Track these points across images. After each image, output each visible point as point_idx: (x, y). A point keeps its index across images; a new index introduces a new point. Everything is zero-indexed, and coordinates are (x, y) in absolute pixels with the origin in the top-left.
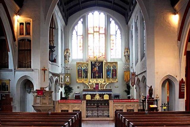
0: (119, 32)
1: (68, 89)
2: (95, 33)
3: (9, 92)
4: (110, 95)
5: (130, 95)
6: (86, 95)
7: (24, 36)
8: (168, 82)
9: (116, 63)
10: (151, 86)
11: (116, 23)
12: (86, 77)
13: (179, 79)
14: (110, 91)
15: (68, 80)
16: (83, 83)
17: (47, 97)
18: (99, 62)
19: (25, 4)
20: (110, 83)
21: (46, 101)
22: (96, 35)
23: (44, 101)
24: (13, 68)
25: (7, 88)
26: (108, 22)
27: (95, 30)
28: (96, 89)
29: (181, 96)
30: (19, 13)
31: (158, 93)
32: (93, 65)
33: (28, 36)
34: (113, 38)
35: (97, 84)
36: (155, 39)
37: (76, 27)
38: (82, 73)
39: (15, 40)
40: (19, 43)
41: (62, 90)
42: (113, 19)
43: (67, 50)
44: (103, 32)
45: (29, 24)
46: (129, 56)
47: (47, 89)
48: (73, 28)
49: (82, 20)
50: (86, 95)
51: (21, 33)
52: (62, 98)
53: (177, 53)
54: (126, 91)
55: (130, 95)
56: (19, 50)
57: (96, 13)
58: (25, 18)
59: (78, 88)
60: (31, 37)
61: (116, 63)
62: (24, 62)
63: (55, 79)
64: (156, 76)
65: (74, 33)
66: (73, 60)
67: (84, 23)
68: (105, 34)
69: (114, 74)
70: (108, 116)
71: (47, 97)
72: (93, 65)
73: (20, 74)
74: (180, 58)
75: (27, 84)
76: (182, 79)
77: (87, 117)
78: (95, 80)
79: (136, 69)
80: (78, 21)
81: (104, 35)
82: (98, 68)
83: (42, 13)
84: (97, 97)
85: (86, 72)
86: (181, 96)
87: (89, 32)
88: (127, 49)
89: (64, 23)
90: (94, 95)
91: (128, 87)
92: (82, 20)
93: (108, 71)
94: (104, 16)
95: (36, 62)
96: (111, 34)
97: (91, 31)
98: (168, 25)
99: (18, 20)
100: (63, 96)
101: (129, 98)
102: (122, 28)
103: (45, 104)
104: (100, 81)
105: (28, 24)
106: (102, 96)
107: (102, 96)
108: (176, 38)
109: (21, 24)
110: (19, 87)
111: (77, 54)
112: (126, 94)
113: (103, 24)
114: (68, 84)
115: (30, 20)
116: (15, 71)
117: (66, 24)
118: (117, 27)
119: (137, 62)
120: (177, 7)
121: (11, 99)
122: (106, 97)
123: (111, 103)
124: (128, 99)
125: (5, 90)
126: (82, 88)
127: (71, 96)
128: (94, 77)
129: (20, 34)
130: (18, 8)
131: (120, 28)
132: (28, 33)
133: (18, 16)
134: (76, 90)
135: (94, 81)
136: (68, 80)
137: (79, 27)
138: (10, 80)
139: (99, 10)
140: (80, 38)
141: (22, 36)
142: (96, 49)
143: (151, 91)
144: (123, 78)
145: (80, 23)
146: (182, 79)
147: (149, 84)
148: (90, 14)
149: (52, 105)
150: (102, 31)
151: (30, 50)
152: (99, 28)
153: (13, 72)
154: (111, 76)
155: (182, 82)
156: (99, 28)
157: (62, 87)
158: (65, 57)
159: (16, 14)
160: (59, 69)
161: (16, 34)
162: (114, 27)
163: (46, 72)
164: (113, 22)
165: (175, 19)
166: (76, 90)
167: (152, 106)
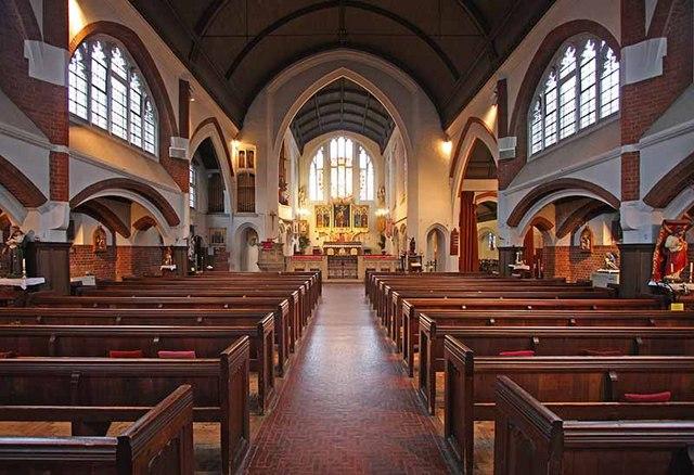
0: (371, 165)
8: (436, 232)
11: (367, 153)
12: (328, 225)
13: (450, 229)
19: (245, 123)
21: (276, 256)
22: (341, 169)
26: (357, 153)
30: (238, 137)
32: (336, 210)
34: (363, 173)
48: (312, 160)
51: (241, 166)
53: (448, 193)
57: (341, 139)
60: (254, 170)
61: (368, 207)
62: (246, 206)
65: (312, 166)
70: (357, 278)
73: (242, 220)
75: (249, 233)
77: (329, 278)
82: (342, 212)
85: (327, 218)
86: (453, 252)
97: (334, 163)
98: (435, 158)
99: (236, 146)
100: (298, 250)
103: (273, 260)
122: (354, 252)
123: (360, 259)
131: (372, 160)
132: (251, 166)
137: (319, 158)
142: (342, 186)
145: (320, 152)
150: (349, 164)
155: (454, 233)
162: (363, 158)
164: (363, 152)
165: (446, 148)
167: (413, 265)
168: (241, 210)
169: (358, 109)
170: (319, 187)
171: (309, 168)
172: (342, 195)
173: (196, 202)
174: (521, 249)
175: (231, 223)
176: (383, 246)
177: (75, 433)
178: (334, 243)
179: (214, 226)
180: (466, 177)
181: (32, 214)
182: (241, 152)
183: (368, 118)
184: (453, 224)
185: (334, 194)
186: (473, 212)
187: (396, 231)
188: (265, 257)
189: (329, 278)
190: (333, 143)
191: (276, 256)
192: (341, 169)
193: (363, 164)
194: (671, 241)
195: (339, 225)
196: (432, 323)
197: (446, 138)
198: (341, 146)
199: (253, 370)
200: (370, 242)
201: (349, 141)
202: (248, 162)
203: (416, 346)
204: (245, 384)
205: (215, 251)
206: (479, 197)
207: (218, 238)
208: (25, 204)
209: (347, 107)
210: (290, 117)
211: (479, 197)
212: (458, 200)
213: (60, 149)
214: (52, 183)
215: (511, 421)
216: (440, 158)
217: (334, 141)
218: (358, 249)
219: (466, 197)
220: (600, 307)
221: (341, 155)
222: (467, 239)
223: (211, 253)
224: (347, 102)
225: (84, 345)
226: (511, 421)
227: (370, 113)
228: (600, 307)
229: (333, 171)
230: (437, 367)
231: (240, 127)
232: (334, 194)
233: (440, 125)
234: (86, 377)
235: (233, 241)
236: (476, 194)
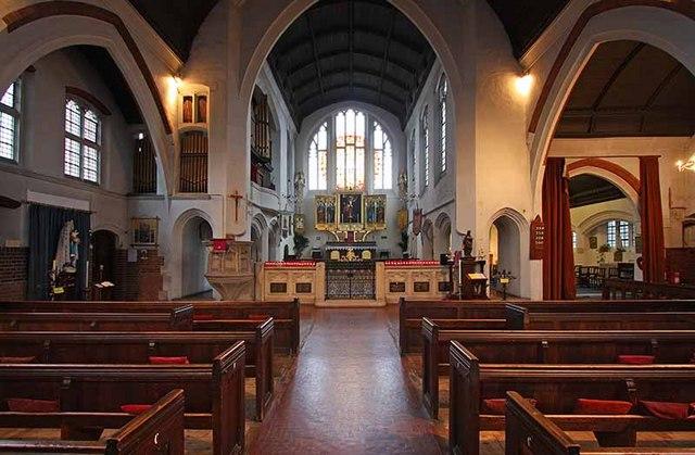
0: (388, 145)
1: (301, 241)
2: (348, 147)
3: (156, 245)
4: (373, 251)
5: (409, 252)
6: (331, 250)
8: (504, 224)
9: (384, 196)
10: (469, 232)
11: (384, 130)
12: (333, 220)
13: (529, 217)
14: (374, 244)
15: (300, 225)
16: (327, 232)
18: (355, 196)
19: (193, 53)
20: (372, 232)
22: (350, 150)
23: (229, 265)
24: (166, 194)
25: (153, 235)
26: (370, 130)
27: (348, 142)
28: (349, 241)
29: (533, 257)
30: (180, 73)
31: (487, 246)
32: (344, 200)
33: (199, 125)
34: (379, 155)
35: (350, 233)
37: (315, 138)
38: (325, 215)
39: (168, 130)
40: (182, 142)
41: (289, 241)
42: (379, 123)
44: (362, 145)
46: (406, 185)
47: (247, 238)
48: (312, 139)
49: (326, 124)
50: (331, 250)
52: (287, 258)
54: (400, 245)
55: (409, 252)
56: (183, 156)
57: (350, 113)
58: (197, 85)
59: (319, 239)
60: (206, 126)
61: (384, 196)
62: (193, 181)
63: (269, 221)
65: (313, 146)
66: (310, 192)
69: (381, 217)
70: (374, 298)
73: (184, 205)
75: (200, 227)
76: (538, 216)
77: (327, 298)
79: (426, 205)
80: (320, 126)
81: (363, 150)
82: (352, 205)
84: (351, 256)
85: (332, 211)
89: (293, 127)
90: (346, 251)
91: (405, 238)
92: (326, 124)
93: (370, 209)
94: (363, 117)
95: (218, 180)
96: (376, 147)
97: (340, 143)
98: (503, 105)
99: (175, 90)
100: (291, 252)
101: (406, 258)
102: (393, 136)
103: (233, 270)
104: (356, 228)
105: (201, 98)
106: (358, 253)
107: (358, 253)
108: (524, 129)
110: (181, 232)
113: (361, 132)
114: (300, 232)
115: (205, 90)
116: (170, 199)
117: (299, 131)
118: (386, 137)
119: (424, 189)
120: (529, 57)
121: (161, 261)
122: (366, 255)
123: (379, 266)
124: (403, 260)
125: (148, 241)
126: (325, 239)
127: (306, 253)
128: (345, 220)
129: (185, 121)
130: (177, 62)
131: (390, 138)
132: (201, 119)
133: (178, 79)
134: (315, 243)
135: (345, 228)
136: (300, 225)
137: (321, 137)
138: (157, 219)
139: (356, 110)
140: (323, 155)
141: (188, 125)
142: (350, 172)
143: (468, 242)
144: (396, 222)
145: (322, 129)
146: (538, 216)
147: (460, 226)
149: (250, 273)
150: (360, 143)
151: (206, 156)
152: (355, 138)
153: (167, 200)
154: (374, 218)
155: (535, 223)
156: (355, 138)
157: (285, 236)
158: (296, 186)
159: (174, 75)
160: (279, 201)
161: (170, 118)
162: (379, 136)
163: (242, 202)
164: (378, 128)
165: (522, 88)
166: (315, 243)
167: (473, 276)
168: (183, 189)
169: (376, 63)
171: (309, 149)
172: (351, 183)
173: (101, 172)
175: (168, 210)
176: (404, 247)
177: (64, 437)
179: (138, 216)
180: (557, 135)
182: (187, 98)
183: (387, 77)
184: (531, 207)
185: (340, 183)
186: (564, 189)
187: (428, 224)
188: (216, 264)
189: (327, 298)
190: (340, 118)
192: (350, 150)
193: (378, 144)
196: (434, 327)
198: (350, 122)
199: (250, 374)
201: (360, 114)
204: (240, 387)
205: (140, 254)
206: (573, 167)
207: (144, 234)
208: (15, 207)
209: (359, 58)
210: (268, 45)
211: (573, 167)
212: (542, 168)
215: (518, 426)
217: (341, 114)
218: (372, 251)
219: (554, 166)
221: (350, 132)
222: (552, 240)
223: (133, 257)
224: (359, 85)
225: (85, 351)
226: (518, 426)
227: (389, 67)
229: (340, 152)
230: (442, 372)
231: (184, 57)
232: (340, 183)
233: (510, 51)
234: (78, 382)
235: (171, 240)
236: (568, 162)
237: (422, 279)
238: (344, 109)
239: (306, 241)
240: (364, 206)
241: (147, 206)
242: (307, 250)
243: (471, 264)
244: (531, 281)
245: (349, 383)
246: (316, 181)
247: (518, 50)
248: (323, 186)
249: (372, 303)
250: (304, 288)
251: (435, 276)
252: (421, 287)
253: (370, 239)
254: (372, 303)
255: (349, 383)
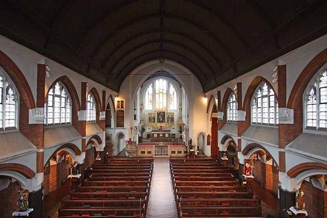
0: (175, 93)
4: (169, 134)
7: (120, 109)
8: (202, 135)
9: (173, 113)
12: (154, 122)
13: (207, 134)
17: (134, 145)
19: (120, 90)
21: (133, 147)
22: (161, 95)
24: (114, 127)
26: (169, 86)
29: (208, 144)
30: (117, 96)
32: (159, 114)
33: (122, 109)
34: (172, 96)
36: (194, 112)
37: (148, 89)
38: (151, 119)
43: (142, 105)
44: (166, 93)
45: (123, 101)
48: (146, 90)
51: (118, 107)
53: (206, 119)
56: (117, 117)
57: (161, 80)
60: (124, 109)
61: (173, 113)
62: (120, 124)
64: (194, 133)
65: (147, 93)
67: (153, 87)
68: (167, 94)
69: (172, 119)
70: (167, 155)
71: (134, 145)
72: (159, 114)
73: (118, 130)
74: (208, 121)
77: (155, 155)
78: (160, 124)
82: (161, 116)
83: (130, 96)
85: (154, 119)
86: (208, 144)
87: (156, 92)
88: (181, 104)
95: (127, 124)
97: (157, 92)
98: (200, 105)
99: (117, 99)
104: (163, 125)
105: (122, 102)
109: (118, 102)
111: (148, 107)
112: (179, 133)
118: (174, 89)
126: (151, 129)
128: (159, 121)
131: (176, 90)
132: (122, 107)
135: (159, 125)
139: (163, 79)
140: (151, 96)
142: (161, 105)
145: (150, 86)
148: (157, 81)
150: (165, 92)
158: (141, 109)
162: (172, 89)
163: (133, 129)
164: (172, 86)
166: (148, 130)
167: (191, 150)
168: (118, 126)
170: (150, 103)
174: (225, 152)
178: (157, 131)
181: (78, 156)
184: (208, 132)
189: (155, 155)
191: (133, 147)
192: (161, 95)
194: (247, 164)
195: (160, 122)
197: (205, 96)
200: (175, 131)
202: (121, 105)
203: (180, 190)
213: (84, 138)
214: (82, 148)
216: (203, 105)
219: (214, 120)
220: (226, 184)
221: (161, 88)
228: (226, 184)
229: (157, 95)
231: (118, 92)
237: (178, 151)
238: (159, 79)
239: (145, 129)
240: (166, 116)
241: (110, 131)
242: (144, 133)
243: (191, 147)
244: (208, 151)
245: (162, 188)
246: (148, 107)
247: (205, 92)
248: (151, 108)
249: (167, 156)
250: (149, 152)
251: (182, 149)
252: (180, 152)
253: (168, 129)
254: (167, 156)
255: (162, 188)
